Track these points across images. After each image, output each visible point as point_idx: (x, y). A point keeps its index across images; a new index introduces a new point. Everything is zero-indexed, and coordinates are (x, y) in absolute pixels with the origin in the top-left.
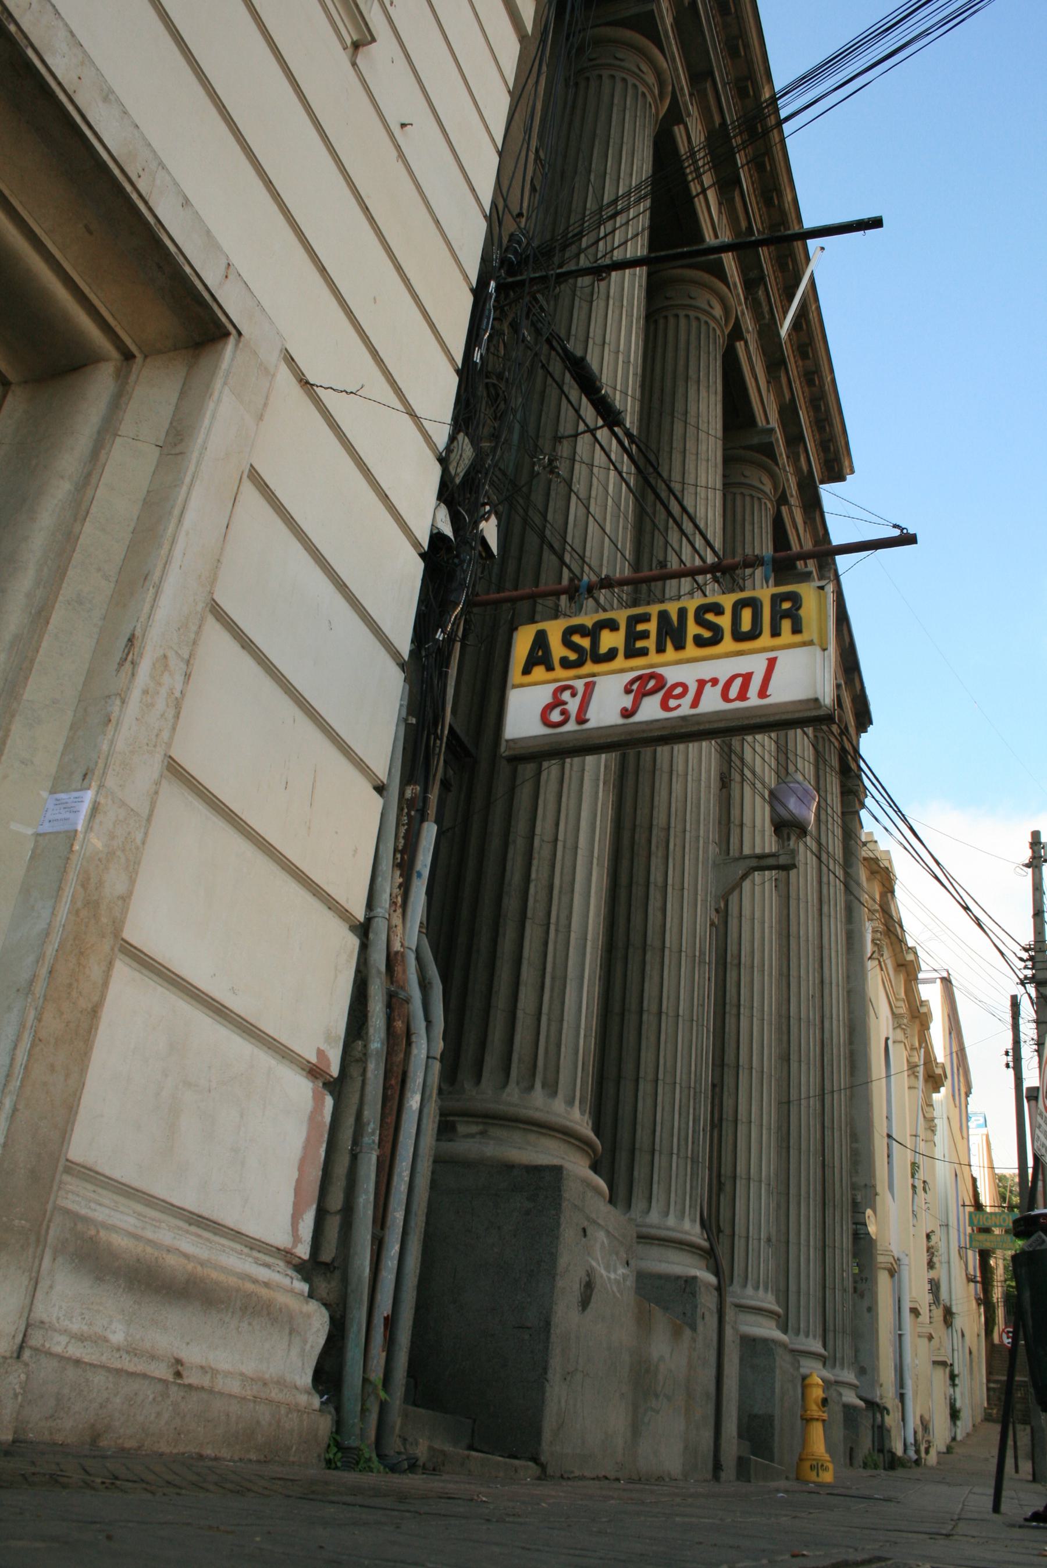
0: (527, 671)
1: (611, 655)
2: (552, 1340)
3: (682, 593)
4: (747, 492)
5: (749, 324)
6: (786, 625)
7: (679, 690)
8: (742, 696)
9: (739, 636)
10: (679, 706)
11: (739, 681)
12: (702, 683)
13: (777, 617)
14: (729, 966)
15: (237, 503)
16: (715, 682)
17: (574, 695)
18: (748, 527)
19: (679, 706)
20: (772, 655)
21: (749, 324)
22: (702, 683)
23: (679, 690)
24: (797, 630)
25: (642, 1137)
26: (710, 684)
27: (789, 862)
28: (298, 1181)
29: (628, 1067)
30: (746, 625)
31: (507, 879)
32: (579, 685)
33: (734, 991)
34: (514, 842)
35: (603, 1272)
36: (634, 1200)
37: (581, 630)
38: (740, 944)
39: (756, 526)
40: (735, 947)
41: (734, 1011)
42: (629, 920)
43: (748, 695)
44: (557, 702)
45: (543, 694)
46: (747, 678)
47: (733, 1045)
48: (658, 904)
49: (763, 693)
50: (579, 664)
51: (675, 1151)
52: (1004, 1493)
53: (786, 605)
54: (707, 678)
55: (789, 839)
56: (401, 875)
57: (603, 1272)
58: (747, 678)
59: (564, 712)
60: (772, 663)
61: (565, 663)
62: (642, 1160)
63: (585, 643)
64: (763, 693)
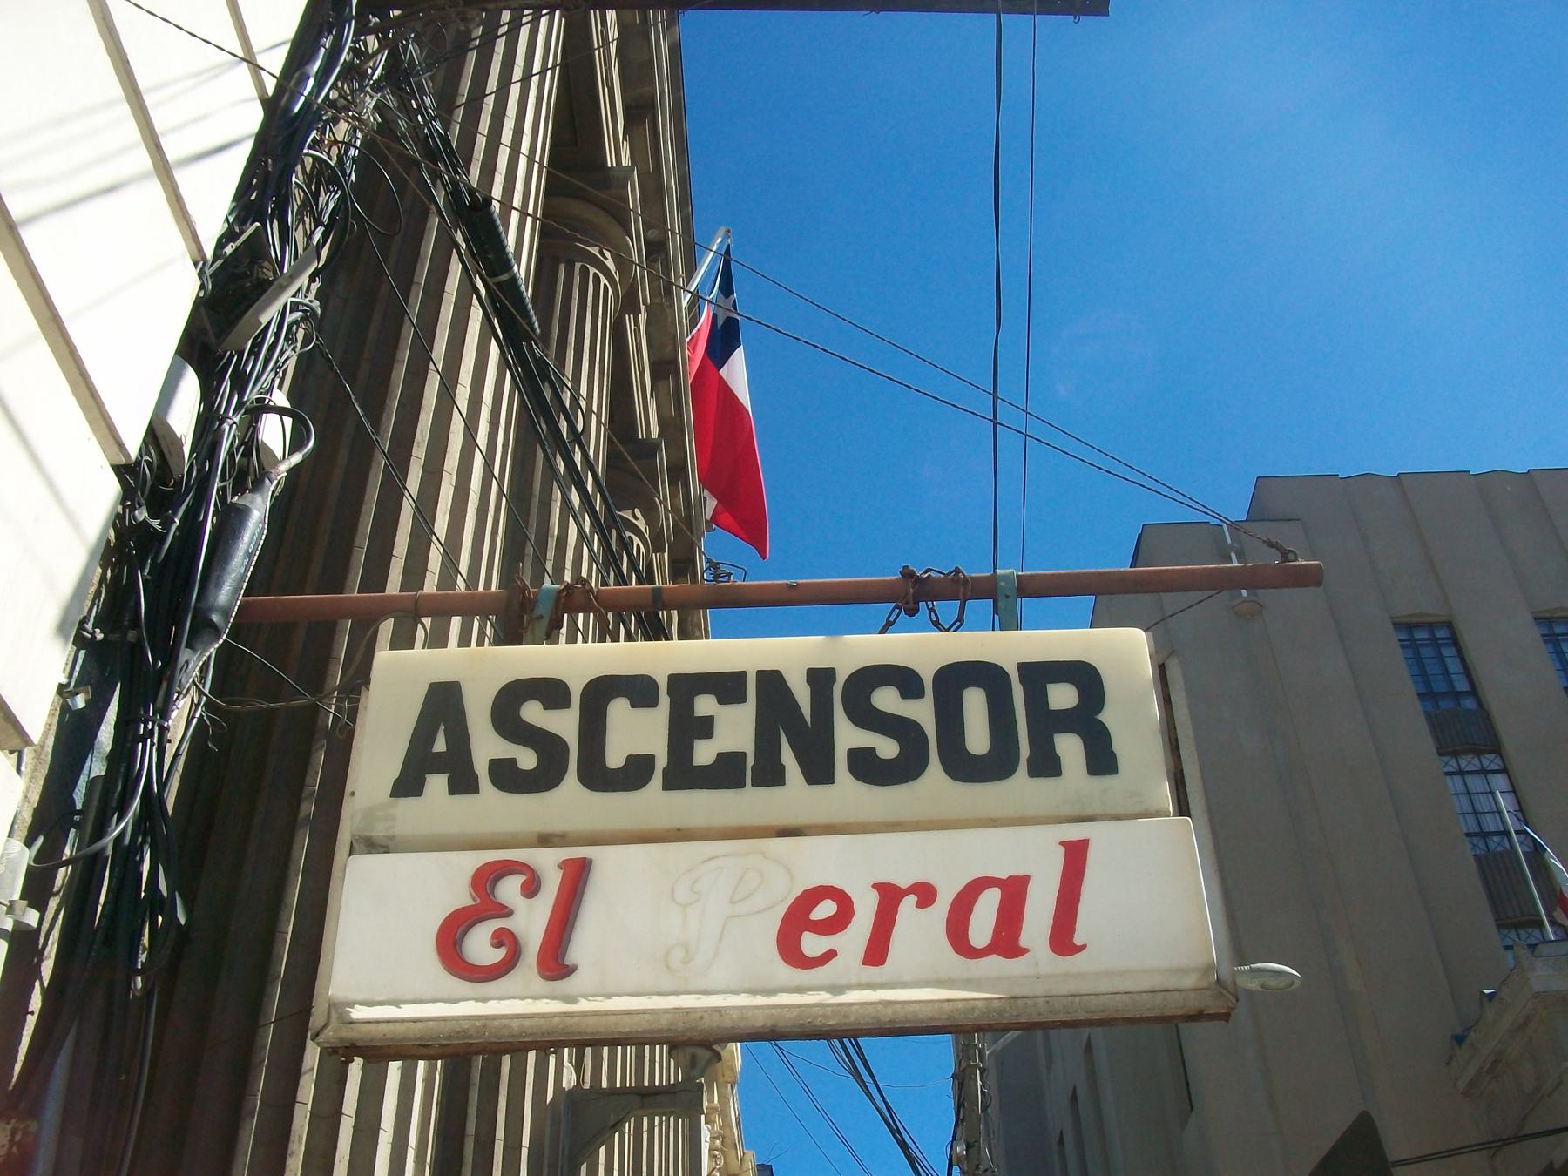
0: (408, 785)
1: (636, 772)
3: (1469, 778)
5: (645, 293)
6: (1069, 747)
7: (826, 909)
8: (1007, 941)
9: (963, 767)
10: (831, 954)
11: (989, 902)
12: (889, 896)
13: (1047, 723)
15: (1088, 812)
16: (925, 894)
17: (531, 888)
19: (831, 954)
20: (1074, 832)
21: (645, 293)
22: (889, 896)
23: (826, 909)
26: (911, 900)
30: (978, 738)
32: (548, 862)
37: (551, 692)
43: (1024, 941)
44: (486, 902)
45: (443, 882)
49: (1063, 939)
50: (544, 779)
52: (149, 100)
53: (1062, 696)
54: (904, 883)
58: (1014, 891)
59: (503, 938)
60: (1076, 855)
61: (506, 776)
63: (565, 724)
64: (1063, 939)
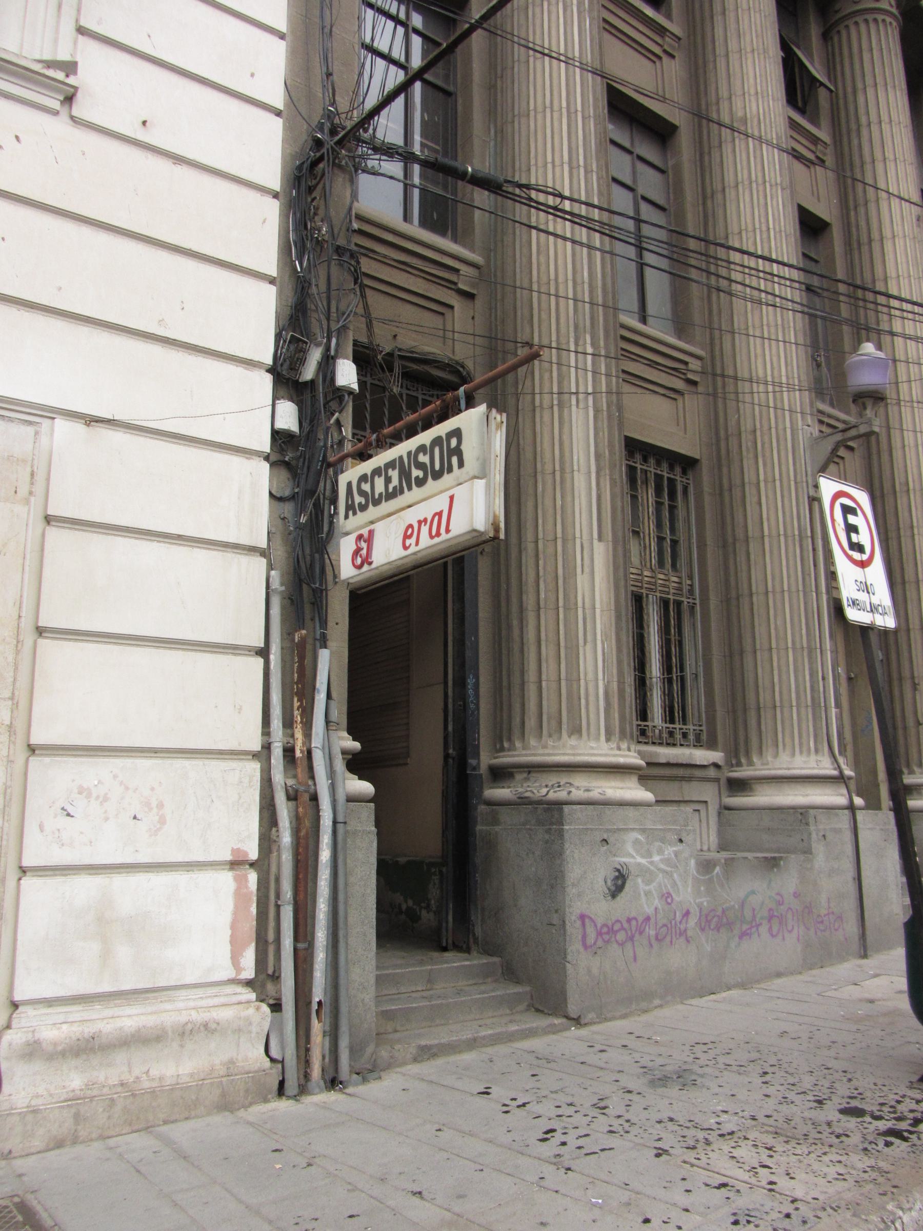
2: (568, 933)
4: (870, 17)
11: (437, 518)
12: (420, 522)
14: (898, 494)
18: (866, 56)
20: (450, 493)
24: (461, 464)
25: (765, 697)
27: (868, 430)
28: (232, 936)
29: (747, 641)
31: (524, 580)
33: (906, 514)
34: (525, 549)
35: (643, 861)
36: (764, 748)
38: (906, 471)
39: (875, 52)
40: (903, 475)
41: (909, 533)
42: (733, 518)
46: (440, 514)
47: (911, 565)
48: (755, 499)
51: (794, 704)
55: (865, 408)
56: (298, 700)
57: (643, 861)
62: (766, 717)
64: (448, 531)
